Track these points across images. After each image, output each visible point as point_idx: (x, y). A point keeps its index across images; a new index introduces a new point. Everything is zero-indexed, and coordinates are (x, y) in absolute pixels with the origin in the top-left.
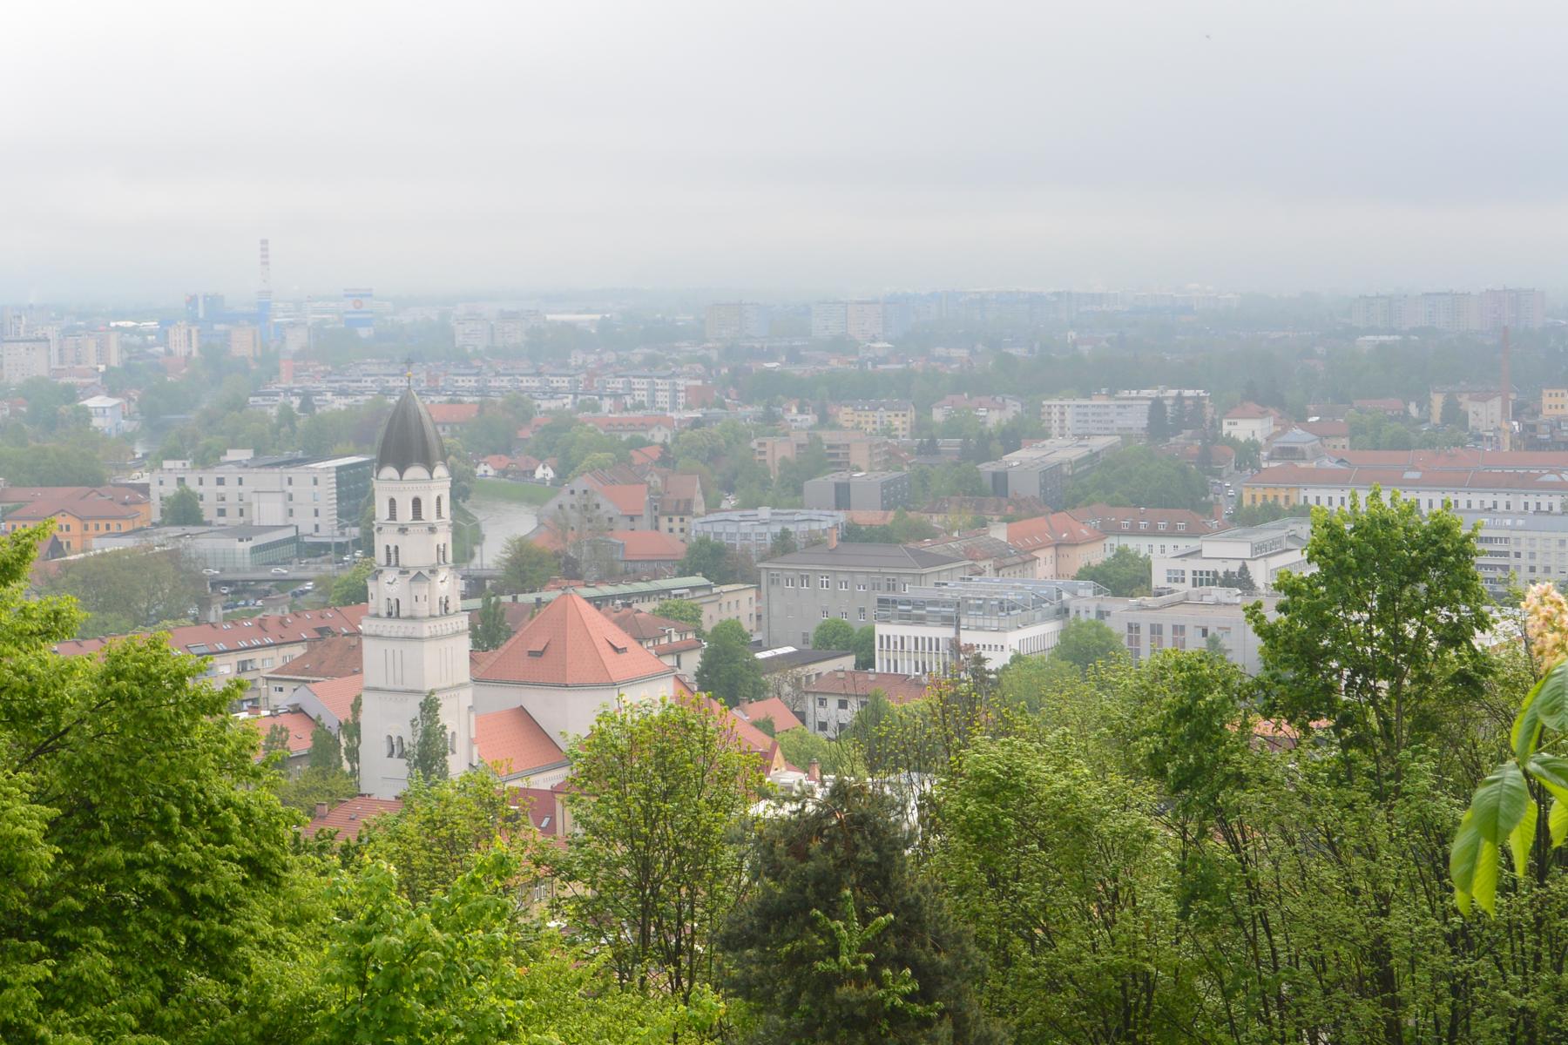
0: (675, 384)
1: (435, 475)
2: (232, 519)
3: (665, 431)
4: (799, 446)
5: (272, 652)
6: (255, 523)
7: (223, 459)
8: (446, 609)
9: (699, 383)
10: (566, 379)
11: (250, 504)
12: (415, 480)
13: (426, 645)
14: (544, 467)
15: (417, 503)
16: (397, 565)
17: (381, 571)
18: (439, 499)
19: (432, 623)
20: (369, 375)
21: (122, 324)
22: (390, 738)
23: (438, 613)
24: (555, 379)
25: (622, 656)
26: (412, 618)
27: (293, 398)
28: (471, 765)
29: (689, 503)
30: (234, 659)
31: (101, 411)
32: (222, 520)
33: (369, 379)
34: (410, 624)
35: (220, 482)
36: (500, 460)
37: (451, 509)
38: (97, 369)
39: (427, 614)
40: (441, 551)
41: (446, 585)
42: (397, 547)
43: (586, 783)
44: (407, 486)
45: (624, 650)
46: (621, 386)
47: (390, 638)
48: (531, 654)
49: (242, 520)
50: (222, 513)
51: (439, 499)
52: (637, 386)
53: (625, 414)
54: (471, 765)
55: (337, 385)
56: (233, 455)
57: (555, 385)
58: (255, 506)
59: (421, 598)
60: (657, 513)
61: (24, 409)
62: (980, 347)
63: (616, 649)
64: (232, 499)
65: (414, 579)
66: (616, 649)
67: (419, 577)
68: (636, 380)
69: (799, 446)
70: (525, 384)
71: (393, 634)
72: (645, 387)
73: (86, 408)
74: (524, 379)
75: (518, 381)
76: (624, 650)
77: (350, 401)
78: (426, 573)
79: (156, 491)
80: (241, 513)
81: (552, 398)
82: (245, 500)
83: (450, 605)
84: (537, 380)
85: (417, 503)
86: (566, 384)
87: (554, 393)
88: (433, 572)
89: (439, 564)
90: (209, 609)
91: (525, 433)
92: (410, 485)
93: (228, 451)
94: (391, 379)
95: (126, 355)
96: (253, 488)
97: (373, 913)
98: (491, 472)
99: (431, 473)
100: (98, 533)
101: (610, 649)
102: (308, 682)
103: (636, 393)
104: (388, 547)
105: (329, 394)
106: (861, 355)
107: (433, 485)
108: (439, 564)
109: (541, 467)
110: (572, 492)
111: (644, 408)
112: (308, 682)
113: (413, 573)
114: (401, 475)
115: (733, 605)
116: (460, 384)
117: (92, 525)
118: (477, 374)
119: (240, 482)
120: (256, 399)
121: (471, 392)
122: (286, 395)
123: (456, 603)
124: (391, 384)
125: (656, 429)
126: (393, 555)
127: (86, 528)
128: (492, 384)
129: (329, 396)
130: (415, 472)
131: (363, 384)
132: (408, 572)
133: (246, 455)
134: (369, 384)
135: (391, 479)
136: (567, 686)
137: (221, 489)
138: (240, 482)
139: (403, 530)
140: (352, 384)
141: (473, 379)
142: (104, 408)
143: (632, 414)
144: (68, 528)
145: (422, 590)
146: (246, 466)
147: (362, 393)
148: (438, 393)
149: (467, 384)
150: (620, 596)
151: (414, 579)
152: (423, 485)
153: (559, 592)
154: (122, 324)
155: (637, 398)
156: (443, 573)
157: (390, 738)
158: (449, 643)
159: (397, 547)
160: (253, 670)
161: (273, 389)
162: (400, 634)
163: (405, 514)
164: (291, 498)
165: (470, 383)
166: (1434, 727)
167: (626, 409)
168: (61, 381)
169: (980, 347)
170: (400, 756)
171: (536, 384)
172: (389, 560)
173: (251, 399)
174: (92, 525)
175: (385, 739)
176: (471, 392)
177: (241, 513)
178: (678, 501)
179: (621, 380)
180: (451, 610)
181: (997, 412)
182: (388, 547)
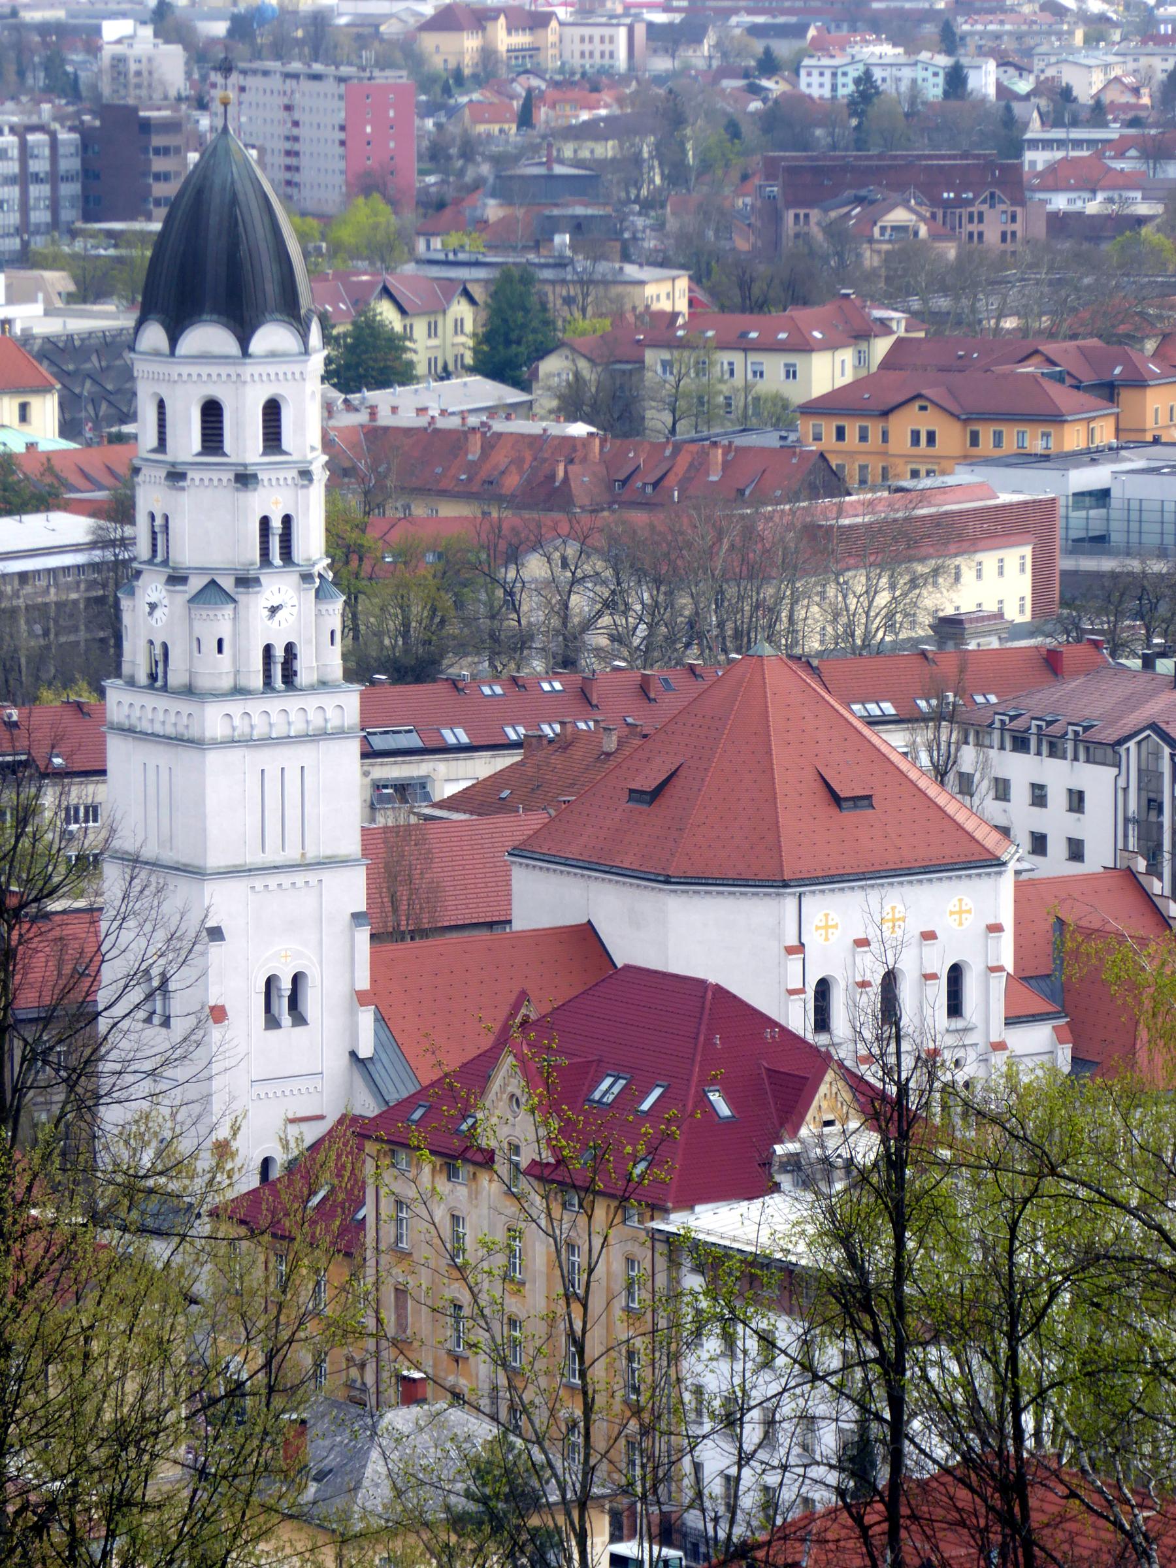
12: (273, 355)
13: (213, 758)
15: (212, 412)
16: (165, 562)
19: (235, 707)
25: (850, 817)
26: (189, 691)
28: (353, 1054)
34: (184, 706)
37: (522, 436)
39: (226, 683)
44: (185, 370)
47: (287, 740)
48: (636, 795)
54: (353, 1054)
63: (837, 800)
65: (196, 599)
66: (837, 800)
67: (212, 593)
71: (158, 729)
78: (227, 583)
85: (212, 412)
92: (194, 370)
97: (628, 1351)
99: (244, 342)
100: (998, 453)
107: (250, 369)
108: (150, 562)
113: (196, 583)
117: (987, 433)
127: (974, 439)
132: (183, 580)
135: (284, 354)
144: (931, 437)
145: (221, 622)
151: (196, 599)
152: (224, 370)
162: (170, 730)
166: (129, 1503)
174: (987, 433)
180: (304, 676)
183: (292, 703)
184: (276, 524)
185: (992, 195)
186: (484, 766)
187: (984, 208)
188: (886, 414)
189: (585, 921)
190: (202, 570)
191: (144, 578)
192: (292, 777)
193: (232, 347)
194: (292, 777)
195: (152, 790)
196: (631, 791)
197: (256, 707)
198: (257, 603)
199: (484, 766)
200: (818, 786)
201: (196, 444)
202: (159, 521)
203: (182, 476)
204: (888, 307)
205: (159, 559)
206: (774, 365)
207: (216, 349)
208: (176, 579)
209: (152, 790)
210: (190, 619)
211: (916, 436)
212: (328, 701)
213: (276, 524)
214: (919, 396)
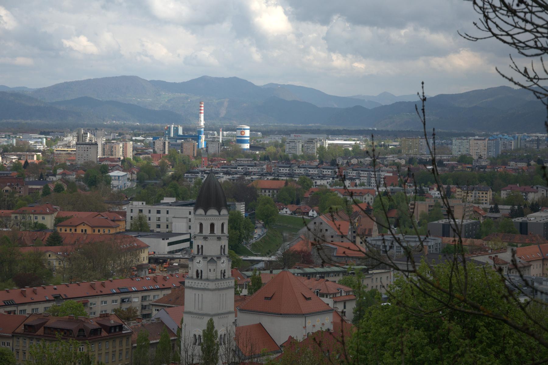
0: (359, 173)
1: (222, 213)
2: (163, 229)
3: (371, 196)
4: (429, 206)
5: (158, 293)
6: (173, 232)
7: (162, 201)
8: (224, 276)
9: (391, 175)
10: (330, 171)
11: (171, 223)
12: (223, 215)
14: (313, 211)
15: (212, 226)
17: (195, 257)
18: (223, 225)
20: (240, 166)
21: (138, 138)
22: (195, 335)
23: (220, 278)
24: (325, 170)
25: (309, 301)
26: (207, 280)
27: (205, 175)
29: (370, 230)
30: (140, 295)
31: (117, 178)
32: (158, 230)
33: (240, 167)
35: (159, 212)
36: (293, 206)
38: (120, 158)
40: (222, 248)
41: (224, 264)
42: (202, 246)
43: (506, 356)
44: (208, 218)
45: (309, 299)
46: (355, 175)
48: (266, 298)
49: (167, 230)
50: (159, 226)
51: (223, 225)
52: (362, 175)
53: (355, 188)
55: (226, 169)
56: (166, 200)
57: (325, 173)
58: (173, 224)
59: (212, 270)
60: (355, 235)
61: (83, 176)
62: (532, 163)
64: (163, 220)
65: (209, 262)
66: (271, 298)
68: (362, 172)
69: (429, 206)
70: (311, 172)
72: (366, 175)
73: (110, 176)
74: (311, 170)
75: (246, 169)
76: (309, 299)
77: (230, 177)
78: (215, 259)
79: (129, 214)
80: (167, 227)
81: (322, 179)
82: (170, 221)
83: (226, 274)
84: (316, 170)
85: (212, 226)
86: (330, 173)
87: (323, 177)
88: (219, 258)
89: (221, 254)
90: (142, 271)
91: (307, 195)
92: (210, 218)
93: (165, 198)
94: (250, 168)
95: (135, 152)
96: (173, 216)
98: (289, 212)
99: (219, 212)
101: (303, 298)
102: (165, 306)
103: (362, 178)
104: (198, 246)
105: (222, 174)
106: (473, 164)
108: (197, 254)
109: (311, 210)
110: (315, 223)
111: (365, 186)
112: (165, 306)
113: (209, 259)
114: (206, 212)
115: (379, 279)
116: (282, 171)
118: (290, 167)
119: (168, 212)
120: (188, 174)
121: (285, 175)
122: (202, 173)
123: (228, 274)
124: (250, 170)
125: (367, 195)
126: (200, 249)
128: (297, 172)
129: (221, 175)
130: (213, 212)
131: (238, 170)
133: (172, 200)
134: (240, 170)
135: (201, 215)
136: (281, 314)
137: (158, 215)
138: (168, 212)
139: (205, 238)
140: (232, 170)
141: (288, 169)
142: (119, 176)
143: (358, 188)
146: (171, 205)
147: (236, 174)
148: (271, 175)
149: (284, 171)
150: (319, 273)
151: (209, 262)
153: (281, 270)
154: (138, 138)
155: (362, 181)
156: (224, 259)
157: (195, 335)
158: (224, 292)
159: (202, 246)
160: (149, 300)
161: (196, 170)
162: (202, 287)
163: (207, 231)
164: (190, 221)
165: (286, 170)
167: (356, 186)
168: (102, 163)
169: (532, 163)
170: (199, 345)
171: (316, 172)
172: (198, 252)
173: (186, 175)
175: (192, 336)
176: (285, 175)
177: (167, 227)
178: (365, 229)
179: (355, 172)
180: (226, 277)
181: (533, 194)
182: (198, 246)
183: (200, 282)
184: (223, 247)
185: (18, 184)
186: (160, 295)
187: (16, 186)
188: (76, 226)
189: (259, 323)
190: (210, 256)
191: (196, 257)
192: (200, 295)
193: (217, 213)
194: (200, 295)
195: (197, 299)
196: (265, 297)
197: (194, 281)
198: (219, 263)
199: (160, 295)
200: (302, 295)
201: (198, 231)
202: (200, 247)
203: (207, 238)
204: (57, 206)
205: (200, 254)
206: (40, 217)
207: (214, 214)
208: (205, 258)
209: (197, 299)
210: (208, 265)
211: (82, 231)
212: (230, 281)
213: (223, 247)
214: (83, 223)
